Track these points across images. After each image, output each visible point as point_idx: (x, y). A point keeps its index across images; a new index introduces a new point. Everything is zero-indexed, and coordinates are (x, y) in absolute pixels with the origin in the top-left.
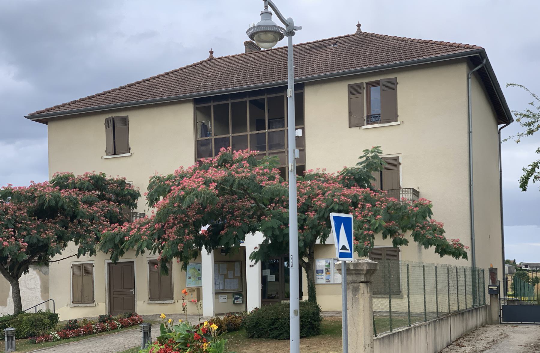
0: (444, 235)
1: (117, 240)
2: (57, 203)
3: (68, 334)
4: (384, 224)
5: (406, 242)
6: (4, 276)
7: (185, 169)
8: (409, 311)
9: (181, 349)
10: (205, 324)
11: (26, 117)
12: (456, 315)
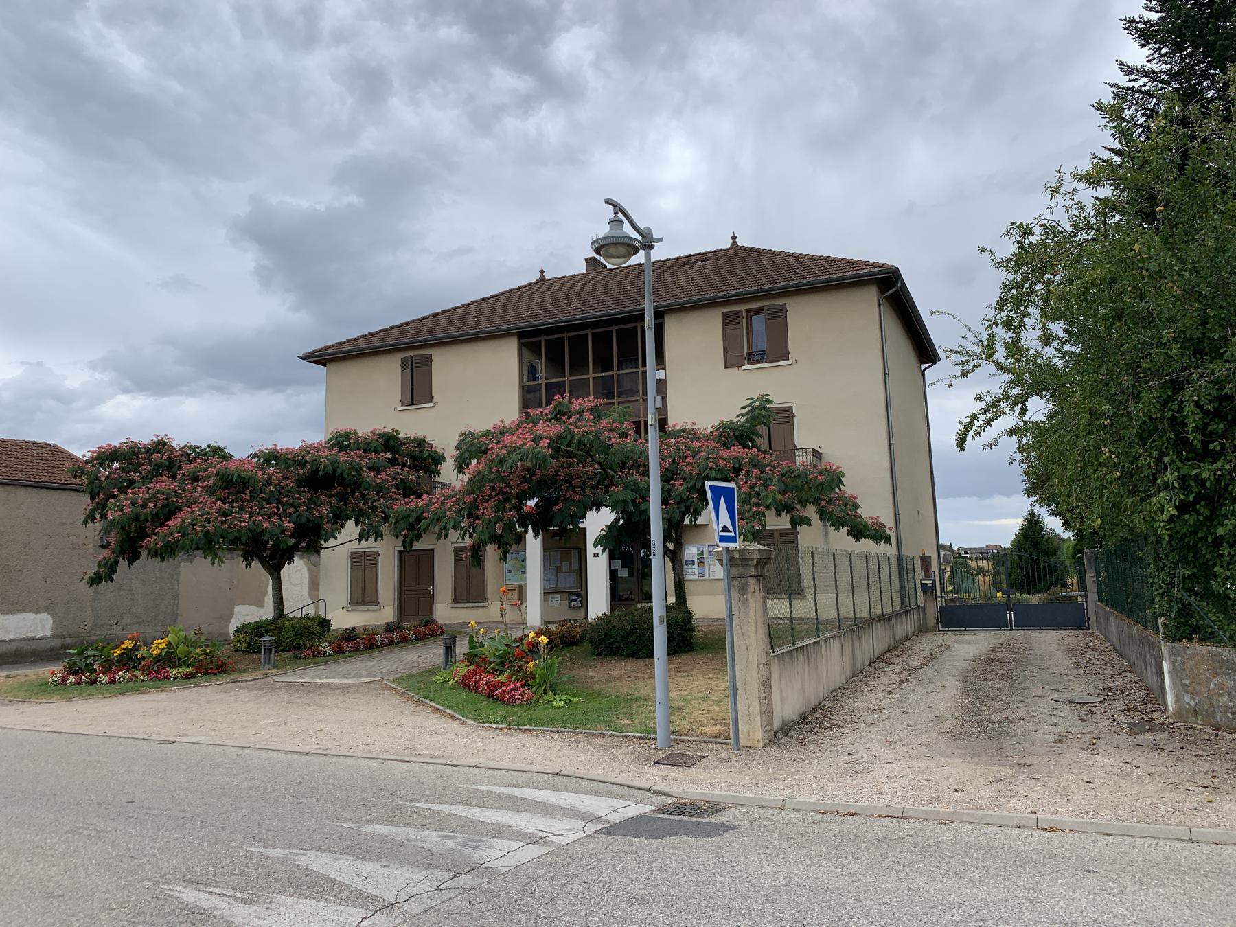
0: (859, 510)
1: (412, 519)
2: (335, 470)
3: (343, 647)
4: (779, 497)
5: (808, 522)
6: (263, 566)
7: (507, 423)
8: (817, 617)
9: (496, 670)
10: (531, 635)
11: (299, 357)
12: (880, 621)
